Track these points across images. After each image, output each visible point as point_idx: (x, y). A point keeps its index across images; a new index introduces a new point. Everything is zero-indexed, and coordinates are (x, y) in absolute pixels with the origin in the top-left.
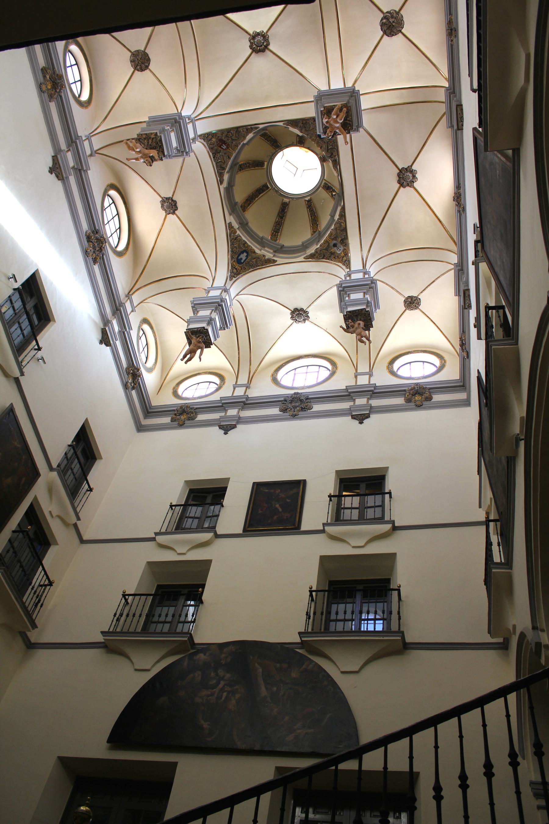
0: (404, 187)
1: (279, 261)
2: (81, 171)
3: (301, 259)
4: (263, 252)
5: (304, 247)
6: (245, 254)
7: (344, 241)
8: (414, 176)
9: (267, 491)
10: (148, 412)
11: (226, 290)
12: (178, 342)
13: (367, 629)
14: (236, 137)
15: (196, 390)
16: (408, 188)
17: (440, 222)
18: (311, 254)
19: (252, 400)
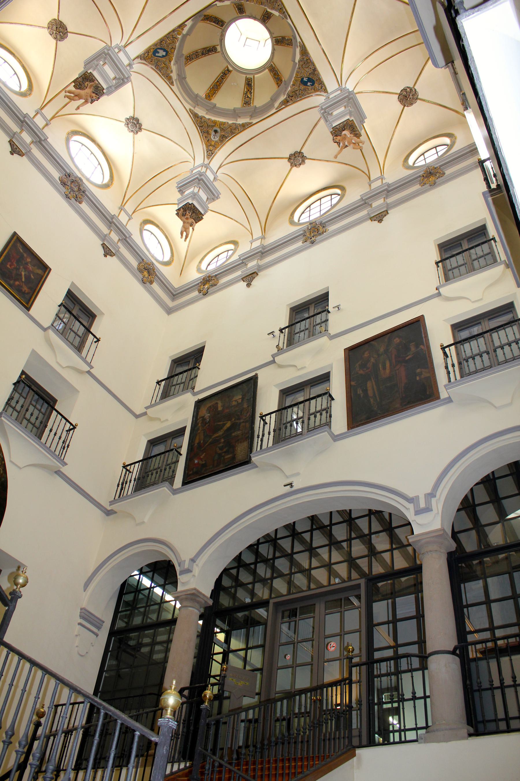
1: (174, 88)
2: (41, 141)
3: (188, 107)
5: (273, 100)
6: (164, 54)
7: (223, 139)
9: (21, 250)
10: (174, 295)
11: (207, 166)
12: (176, 224)
13: (405, 726)
15: (155, 246)
16: (289, 164)
19: (47, 145)
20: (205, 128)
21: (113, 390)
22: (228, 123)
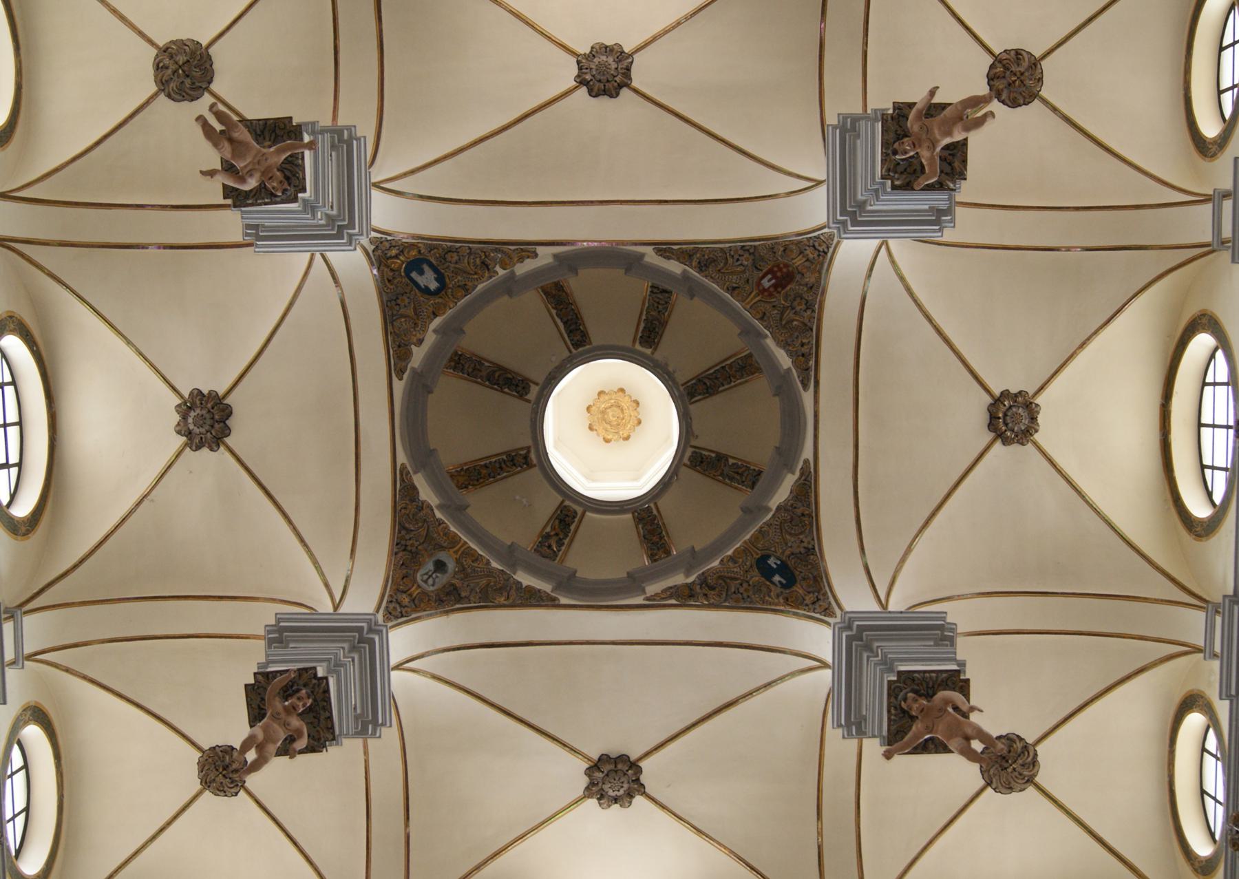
0: (589, 772)
3: (402, 458)
4: (430, 338)
6: (433, 285)
7: (449, 599)
8: (616, 800)
16: (584, 781)
18: (414, 488)
20: (414, 539)
21: (924, 844)
22: (488, 563)
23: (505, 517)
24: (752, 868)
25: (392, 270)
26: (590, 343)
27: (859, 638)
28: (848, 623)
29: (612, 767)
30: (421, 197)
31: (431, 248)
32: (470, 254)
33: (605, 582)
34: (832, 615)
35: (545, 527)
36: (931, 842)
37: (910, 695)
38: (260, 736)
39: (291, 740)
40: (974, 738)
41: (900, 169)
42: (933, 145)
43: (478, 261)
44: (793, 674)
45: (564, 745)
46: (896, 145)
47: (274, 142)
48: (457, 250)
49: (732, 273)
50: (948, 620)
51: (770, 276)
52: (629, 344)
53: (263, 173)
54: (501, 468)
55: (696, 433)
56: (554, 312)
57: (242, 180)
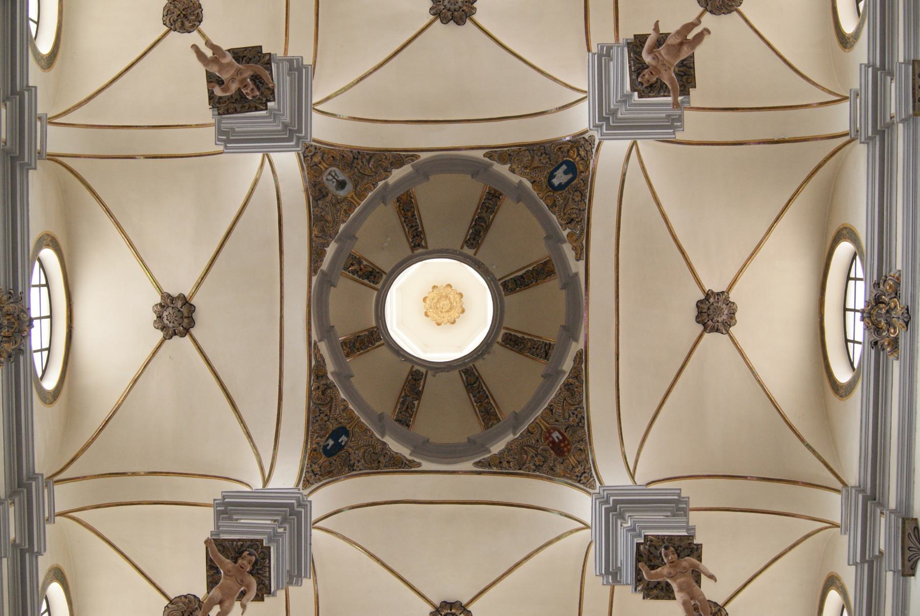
0: (182, 297)
3: (424, 156)
4: (515, 178)
6: (556, 182)
7: (316, 192)
8: (160, 317)
14: (526, 453)
16: (174, 293)
17: (108, 211)
20: (363, 165)
22: (344, 222)
23: (376, 231)
24: (107, 422)
25: (568, 151)
26: (506, 295)
27: (292, 513)
28: (304, 504)
29: (186, 315)
30: (624, 175)
31: (585, 181)
32: (580, 210)
33: (327, 312)
34: (305, 487)
35: (367, 260)
36: (127, 558)
37: (254, 558)
38: (224, 61)
39: (220, 82)
40: (221, 607)
41: (652, 549)
42: (672, 577)
43: (574, 216)
44: (258, 455)
45: (203, 278)
46: (672, 549)
47: (677, 75)
48: (583, 200)
49: (563, 409)
50: (304, 580)
51: (561, 438)
52: (505, 324)
53: (655, 67)
54: (412, 227)
55: (438, 375)
56: (530, 268)
57: (650, 52)
